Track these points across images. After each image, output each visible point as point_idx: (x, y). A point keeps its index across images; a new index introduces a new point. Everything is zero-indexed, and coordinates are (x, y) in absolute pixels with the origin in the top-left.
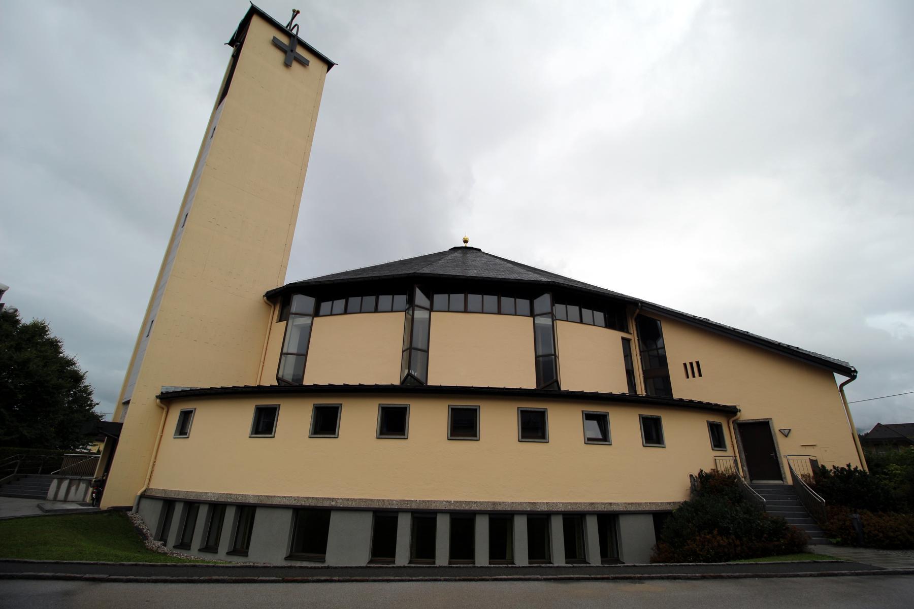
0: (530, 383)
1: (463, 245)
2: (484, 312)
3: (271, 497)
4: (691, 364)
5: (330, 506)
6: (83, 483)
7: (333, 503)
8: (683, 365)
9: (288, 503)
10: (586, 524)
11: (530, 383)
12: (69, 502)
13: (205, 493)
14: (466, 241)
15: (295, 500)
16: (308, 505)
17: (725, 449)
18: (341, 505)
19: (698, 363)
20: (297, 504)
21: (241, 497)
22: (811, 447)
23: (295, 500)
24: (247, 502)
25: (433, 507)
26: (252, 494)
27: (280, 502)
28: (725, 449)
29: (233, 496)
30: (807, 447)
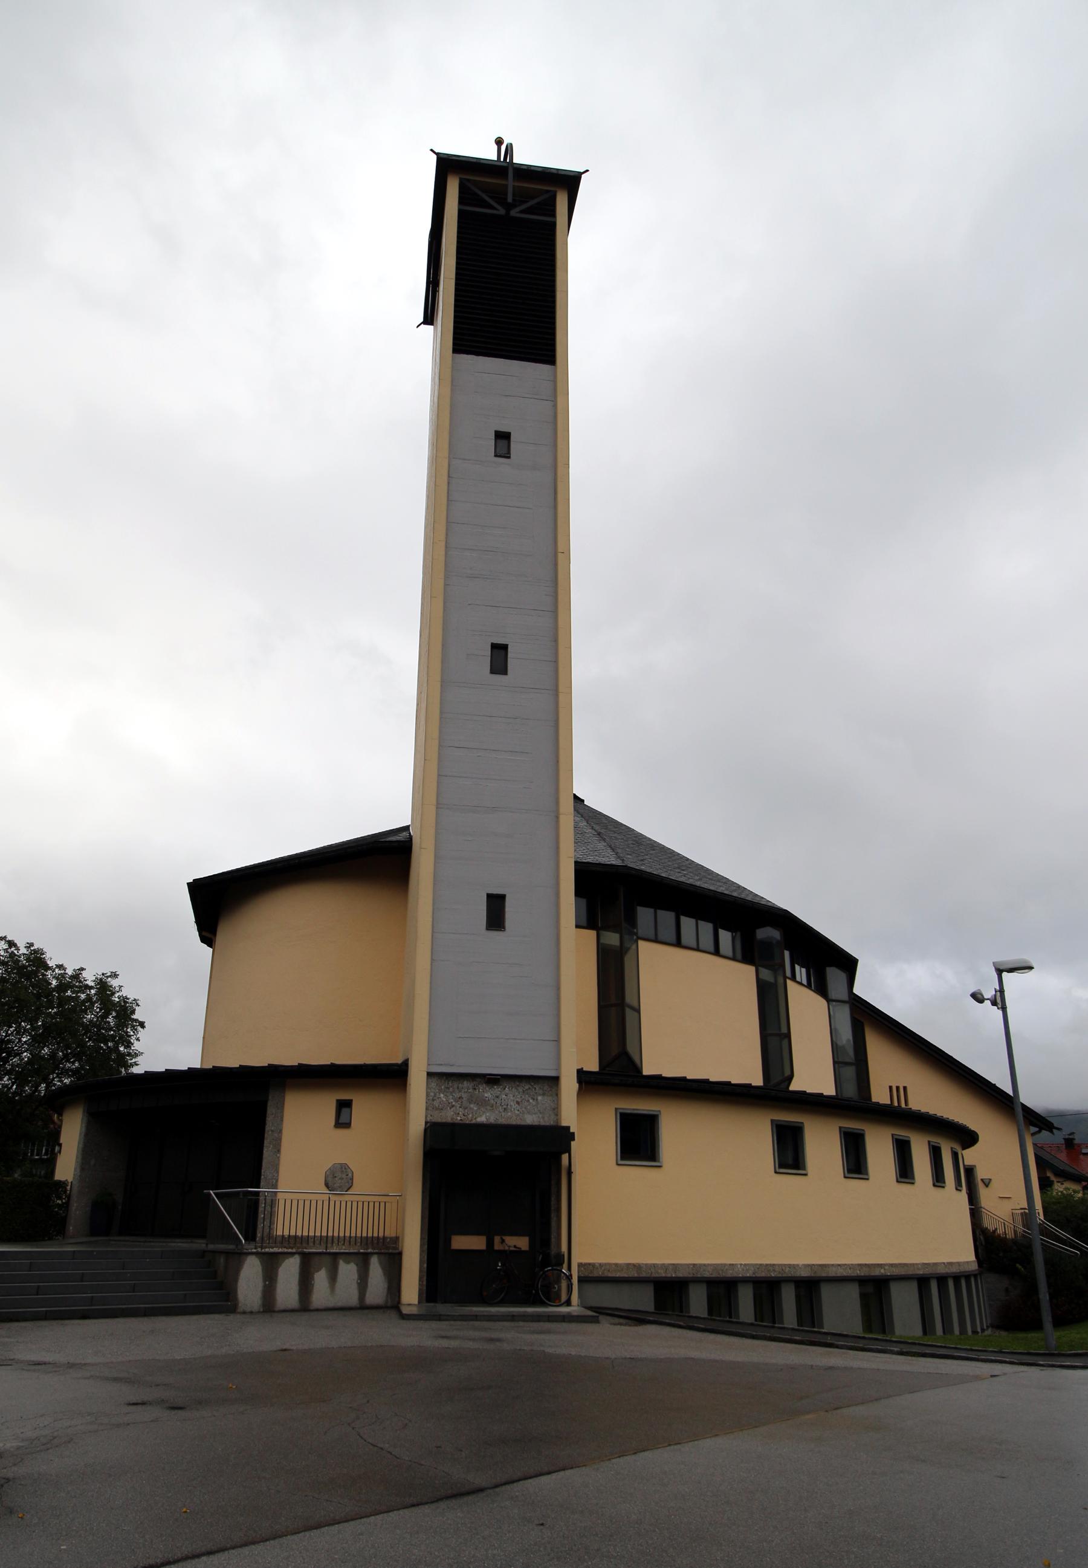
4: (898, 1088)
6: (348, 1263)
7: (882, 1271)
8: (888, 1087)
10: (737, 1297)
12: (244, 1313)
13: (730, 1265)
16: (863, 1274)
17: (943, 1185)
19: (905, 1088)
21: (788, 1269)
24: (798, 1275)
25: (730, 1274)
27: (836, 1274)
28: (943, 1185)
30: (1004, 1200)
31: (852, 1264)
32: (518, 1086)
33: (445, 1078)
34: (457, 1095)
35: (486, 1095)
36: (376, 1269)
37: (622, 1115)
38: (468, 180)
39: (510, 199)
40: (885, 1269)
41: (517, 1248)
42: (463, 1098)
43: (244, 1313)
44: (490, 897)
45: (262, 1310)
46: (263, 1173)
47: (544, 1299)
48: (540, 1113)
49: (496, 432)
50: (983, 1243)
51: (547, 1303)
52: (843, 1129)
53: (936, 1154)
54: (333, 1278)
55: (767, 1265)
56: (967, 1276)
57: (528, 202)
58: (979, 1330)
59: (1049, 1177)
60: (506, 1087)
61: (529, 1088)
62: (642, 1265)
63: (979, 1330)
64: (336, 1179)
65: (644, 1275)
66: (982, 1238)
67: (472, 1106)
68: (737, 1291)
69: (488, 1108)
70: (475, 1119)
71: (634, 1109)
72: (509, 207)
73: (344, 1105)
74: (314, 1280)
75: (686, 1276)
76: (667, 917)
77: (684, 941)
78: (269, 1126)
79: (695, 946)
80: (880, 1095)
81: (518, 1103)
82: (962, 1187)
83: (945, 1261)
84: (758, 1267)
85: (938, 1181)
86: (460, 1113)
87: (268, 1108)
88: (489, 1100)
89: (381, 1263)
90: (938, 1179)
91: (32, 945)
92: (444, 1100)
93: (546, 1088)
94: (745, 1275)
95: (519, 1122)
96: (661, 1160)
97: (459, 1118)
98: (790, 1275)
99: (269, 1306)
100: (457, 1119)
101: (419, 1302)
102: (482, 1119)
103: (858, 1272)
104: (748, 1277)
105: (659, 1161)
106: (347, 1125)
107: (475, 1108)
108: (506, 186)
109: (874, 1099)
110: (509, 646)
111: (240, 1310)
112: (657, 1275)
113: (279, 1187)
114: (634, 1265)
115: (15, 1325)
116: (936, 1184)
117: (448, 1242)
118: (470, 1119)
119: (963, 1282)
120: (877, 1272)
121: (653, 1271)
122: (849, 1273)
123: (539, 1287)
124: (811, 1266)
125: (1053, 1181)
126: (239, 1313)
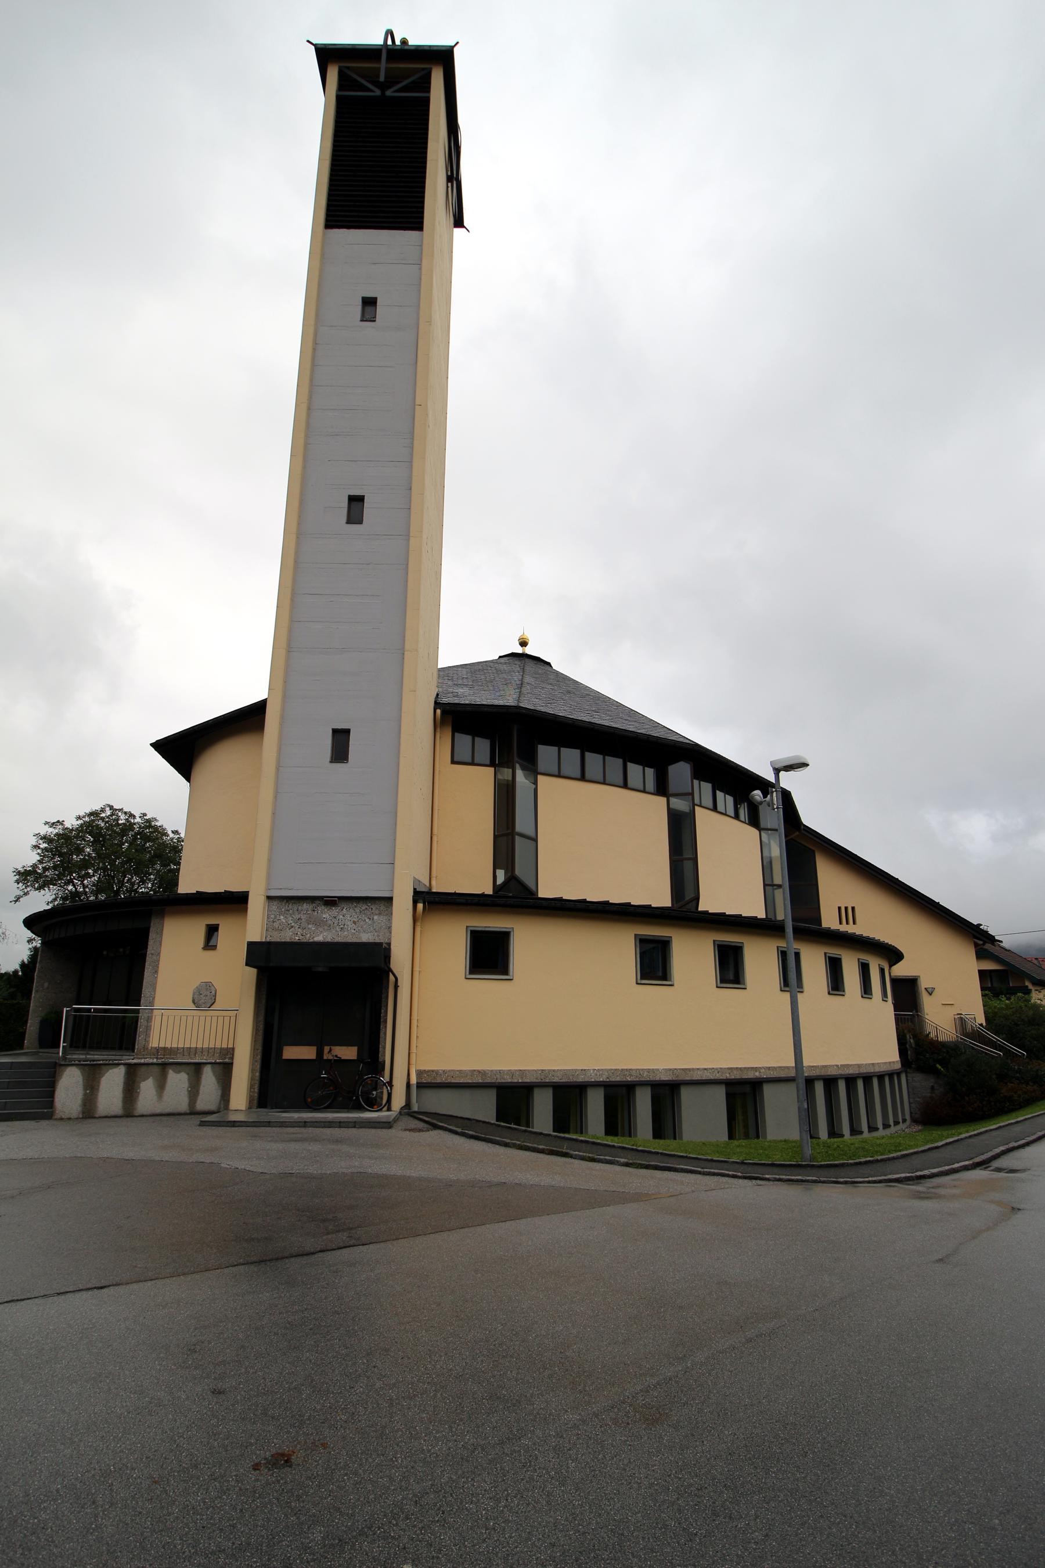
0: (661, 897)
1: (519, 650)
2: (607, 782)
3: (689, 1070)
4: (846, 908)
5: (755, 1077)
7: (757, 1074)
9: (712, 1078)
11: (661, 897)
14: (523, 644)
15: (718, 1072)
16: (733, 1077)
17: (843, 993)
18: (764, 1075)
19: (853, 908)
20: (721, 1078)
22: (949, 1006)
23: (718, 1072)
24: (658, 1079)
25: (581, 1079)
26: (662, 1068)
28: (843, 993)
29: (634, 1072)
30: (947, 1006)
31: (720, 1068)
32: (356, 907)
33: (285, 901)
34: (298, 916)
35: (324, 916)
36: (209, 1079)
37: (472, 932)
38: (348, 68)
39: (382, 78)
40: (760, 1072)
41: (337, 1057)
42: (301, 919)
43: (61, 1119)
44: (335, 732)
45: (81, 1116)
46: (143, 992)
47: (363, 1103)
48: (376, 931)
49: (363, 298)
50: (914, 1046)
51: (365, 1108)
52: (717, 943)
53: (864, 969)
54: (161, 1086)
55: (622, 1070)
56: (891, 1075)
57: (401, 82)
58: (891, 1123)
59: (1027, 986)
60: (344, 908)
61: (366, 909)
62: (487, 1072)
63: (891, 1123)
64: (201, 996)
65: (489, 1080)
66: (912, 1041)
67: (310, 926)
68: (680, 1090)
69: (326, 927)
70: (313, 938)
71: (486, 927)
72: (383, 90)
73: (212, 931)
74: (139, 1088)
75: (533, 1081)
76: (615, 764)
77: (630, 784)
78: (150, 950)
79: (642, 788)
80: (829, 920)
81: (354, 922)
82: (887, 998)
83: (839, 1064)
84: (612, 1071)
85: (865, 993)
86: (299, 933)
87: (150, 934)
88: (327, 921)
89: (214, 1072)
90: (866, 989)
91: (145, 815)
92: (284, 921)
93: (382, 907)
94: (597, 1080)
95: (354, 940)
96: (672, 980)
97: (297, 938)
98: (648, 1079)
99: (88, 1112)
100: (295, 939)
101: (250, 1108)
102: (319, 938)
103: (728, 1075)
104: (601, 1082)
105: (670, 980)
106: (214, 948)
107: (313, 929)
108: (379, 69)
109: (825, 924)
110: (365, 497)
111: (57, 1116)
112: (503, 1081)
113: (155, 1005)
114: (479, 1072)
115: (17, 1124)
116: (865, 996)
117: (280, 1052)
118: (308, 938)
119: (887, 1080)
120: (751, 1075)
121: (498, 1076)
122: (718, 1076)
123: (360, 1093)
124: (672, 1070)
125: (1031, 990)
126: (56, 1119)
